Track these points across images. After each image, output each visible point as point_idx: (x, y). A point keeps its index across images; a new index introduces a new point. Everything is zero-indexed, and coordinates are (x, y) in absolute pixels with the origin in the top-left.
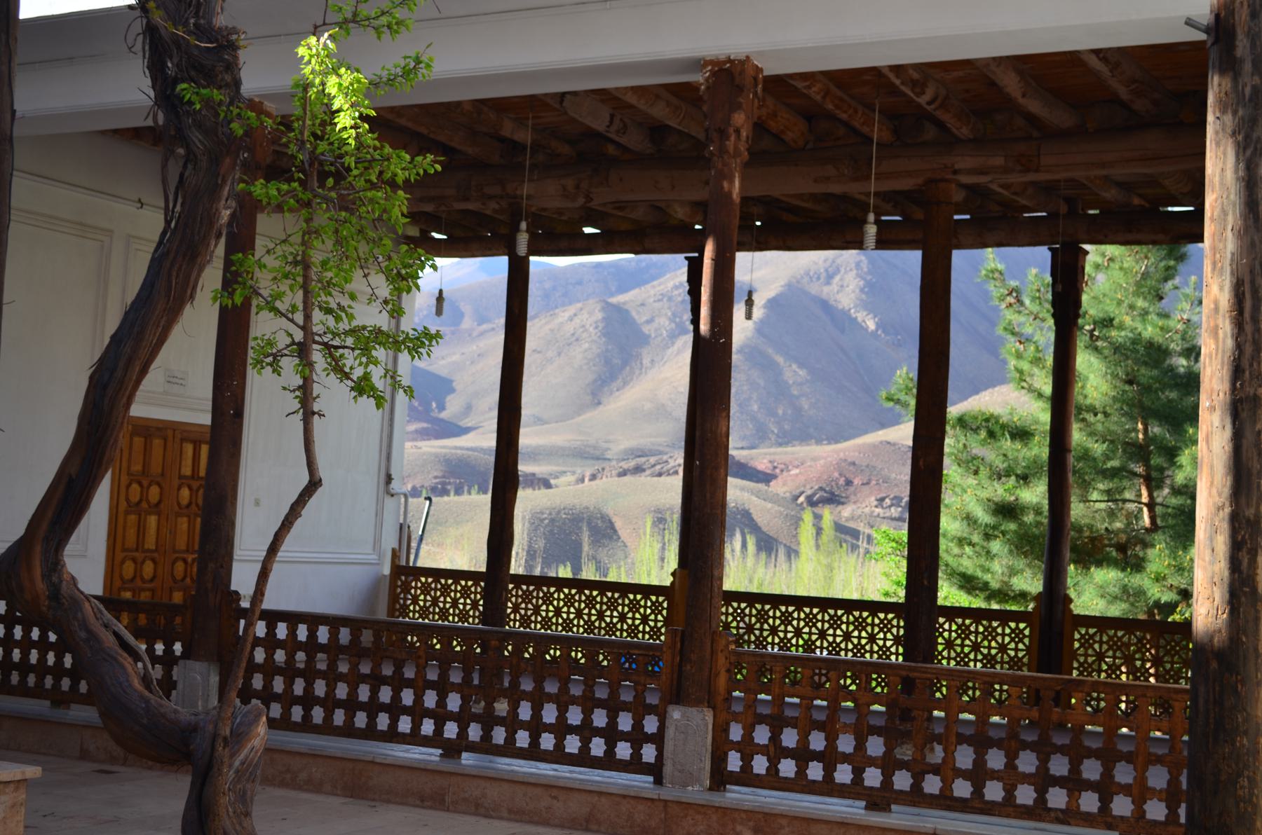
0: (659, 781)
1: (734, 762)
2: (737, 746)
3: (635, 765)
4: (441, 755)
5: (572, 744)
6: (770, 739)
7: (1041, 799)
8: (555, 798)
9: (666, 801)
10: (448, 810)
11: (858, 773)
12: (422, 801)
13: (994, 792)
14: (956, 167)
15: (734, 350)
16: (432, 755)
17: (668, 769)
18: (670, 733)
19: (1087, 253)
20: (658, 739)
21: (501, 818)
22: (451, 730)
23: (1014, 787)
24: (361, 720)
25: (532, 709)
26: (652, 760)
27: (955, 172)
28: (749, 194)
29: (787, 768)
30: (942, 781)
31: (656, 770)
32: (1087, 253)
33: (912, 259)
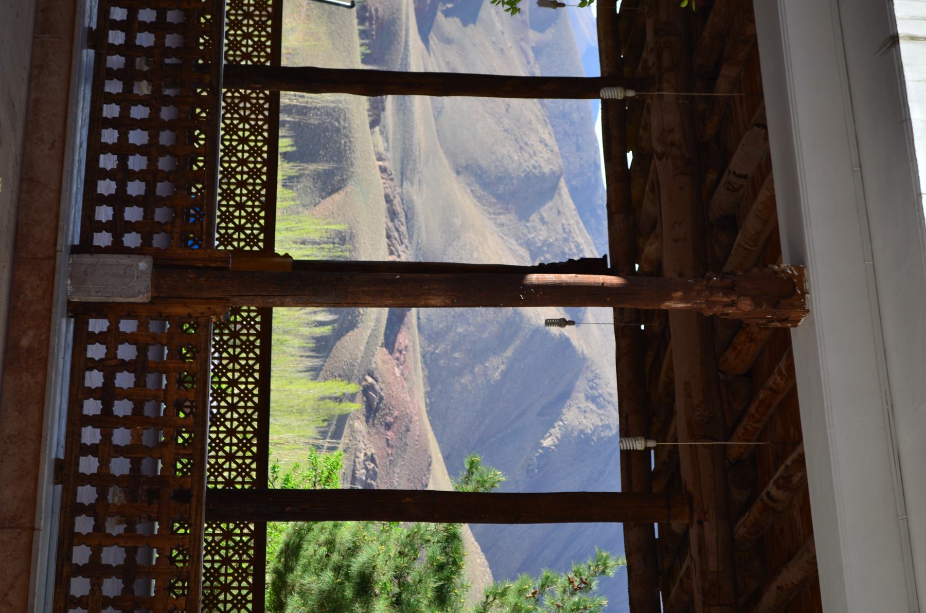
0: (75, 250)
1: (97, 325)
3: (90, 226)
8: (53, 146)
9: (54, 258)
11: (92, 450)
14: (706, 523)
18: (125, 260)
20: (117, 248)
25: (142, 120)
27: (700, 523)
31: (85, 247)
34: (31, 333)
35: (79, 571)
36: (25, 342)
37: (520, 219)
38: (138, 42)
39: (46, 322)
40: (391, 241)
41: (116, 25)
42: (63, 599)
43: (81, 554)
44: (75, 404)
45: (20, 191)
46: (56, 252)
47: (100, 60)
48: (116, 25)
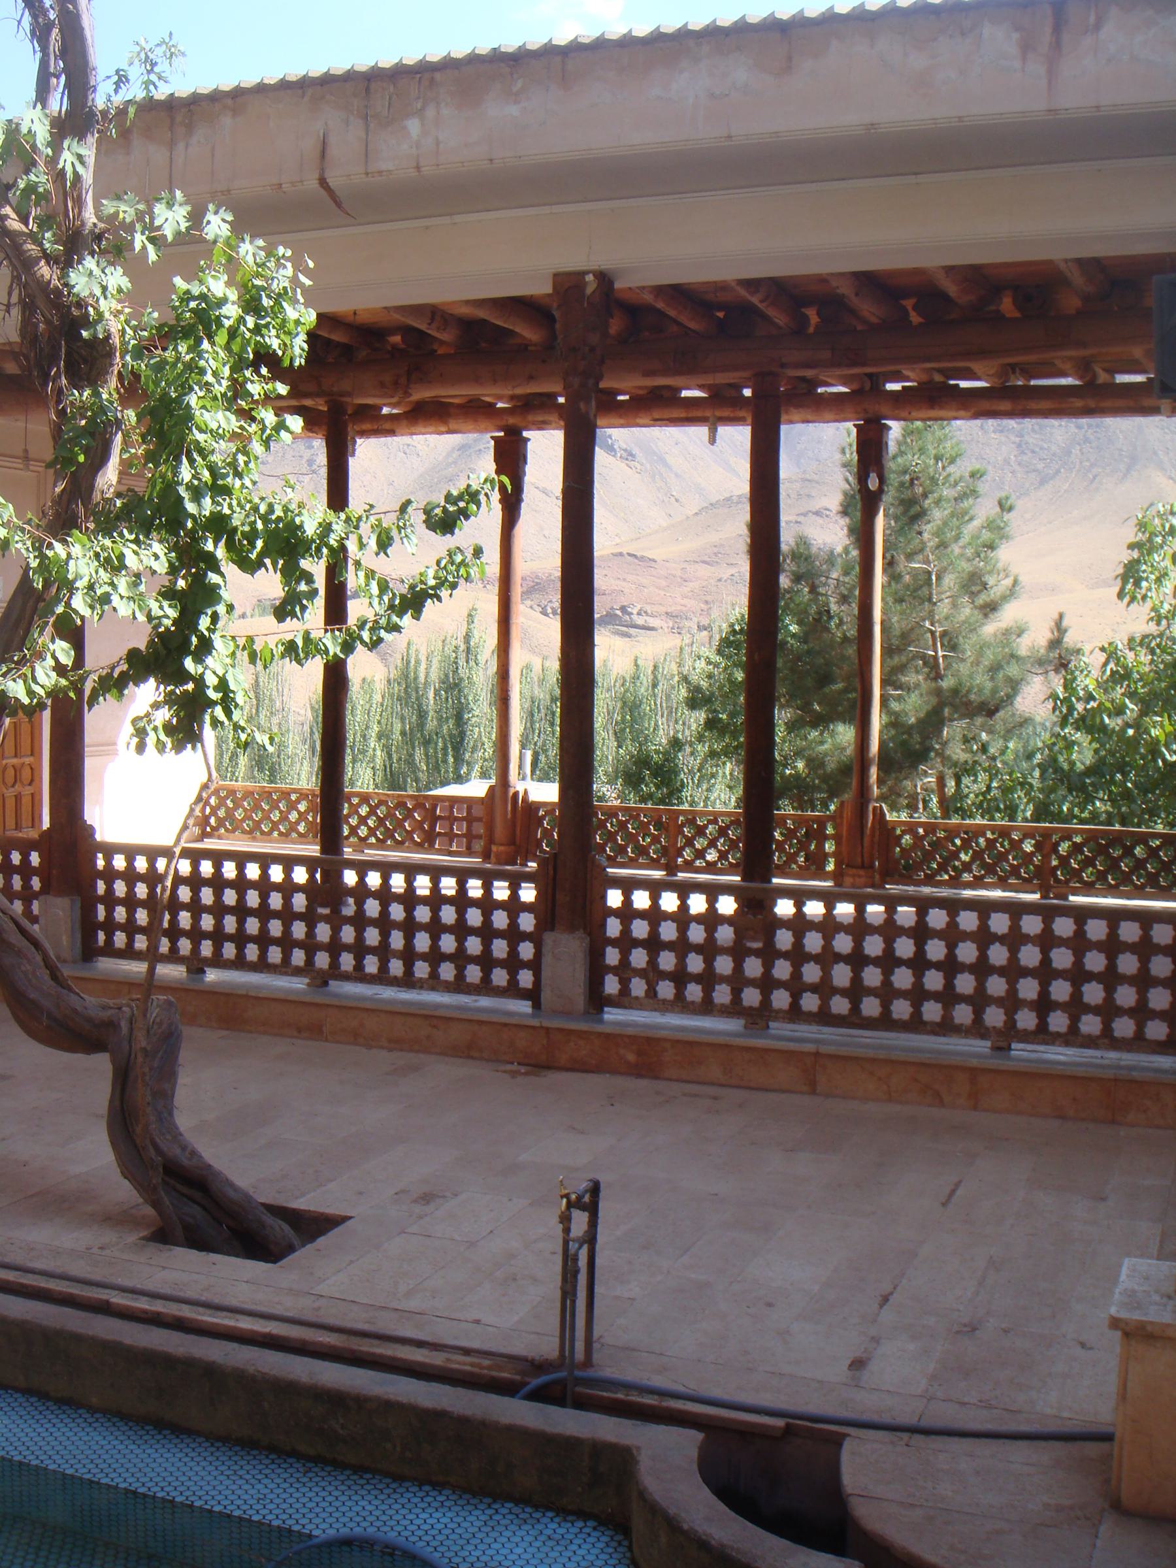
0: (537, 1005)
1: (611, 985)
2: (615, 970)
3: (513, 990)
4: (308, 985)
5: (810, 1002)
6: (648, 963)
7: (917, 1013)
8: (435, 1027)
9: (547, 1029)
10: (327, 1040)
11: (736, 993)
12: (299, 1032)
13: (871, 1007)
14: (784, 360)
15: (492, 451)
16: (299, 984)
17: (546, 995)
18: (547, 960)
19: (889, 428)
20: (535, 965)
21: (382, 1047)
22: (994, 1017)
23: (740, 991)
24: (275, 954)
25: (405, 938)
26: (530, 986)
27: (783, 366)
28: (1155, 1253)
29: (810, 1002)
30: (820, 998)
31: (533, 995)
32: (889, 428)
33: (737, 439)
34: (622, 1051)
35: (855, 1007)
36: (631, 1057)
37: (687, 705)
38: (233, 931)
39: (613, 1039)
40: (195, 469)
41: (310, 961)
42: (1167, 1047)
43: (840, 1006)
44: (665, 1006)
45: (481, 1059)
46: (542, 1027)
47: (1025, 1037)
48: (310, 961)
